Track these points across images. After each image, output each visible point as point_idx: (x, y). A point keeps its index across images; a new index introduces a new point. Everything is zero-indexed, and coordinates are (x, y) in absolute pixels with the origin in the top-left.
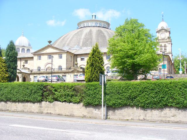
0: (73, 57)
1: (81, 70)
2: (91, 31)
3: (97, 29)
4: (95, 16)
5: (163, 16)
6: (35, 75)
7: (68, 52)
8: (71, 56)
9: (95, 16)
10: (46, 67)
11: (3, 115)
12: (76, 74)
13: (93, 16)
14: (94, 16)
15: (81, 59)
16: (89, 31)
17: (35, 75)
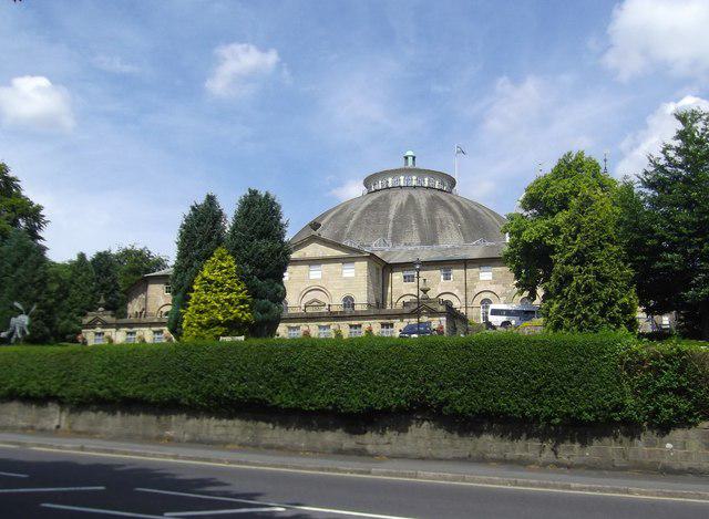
0: (381, 268)
1: (442, 308)
2: (411, 198)
3: (429, 193)
4: (414, 158)
5: (605, 160)
6: (292, 325)
7: (372, 255)
8: (378, 269)
9: (414, 158)
10: (305, 300)
11: (292, 450)
12: (99, 330)
13: (406, 158)
14: (410, 159)
15: (405, 277)
16: (405, 198)
17: (353, 323)
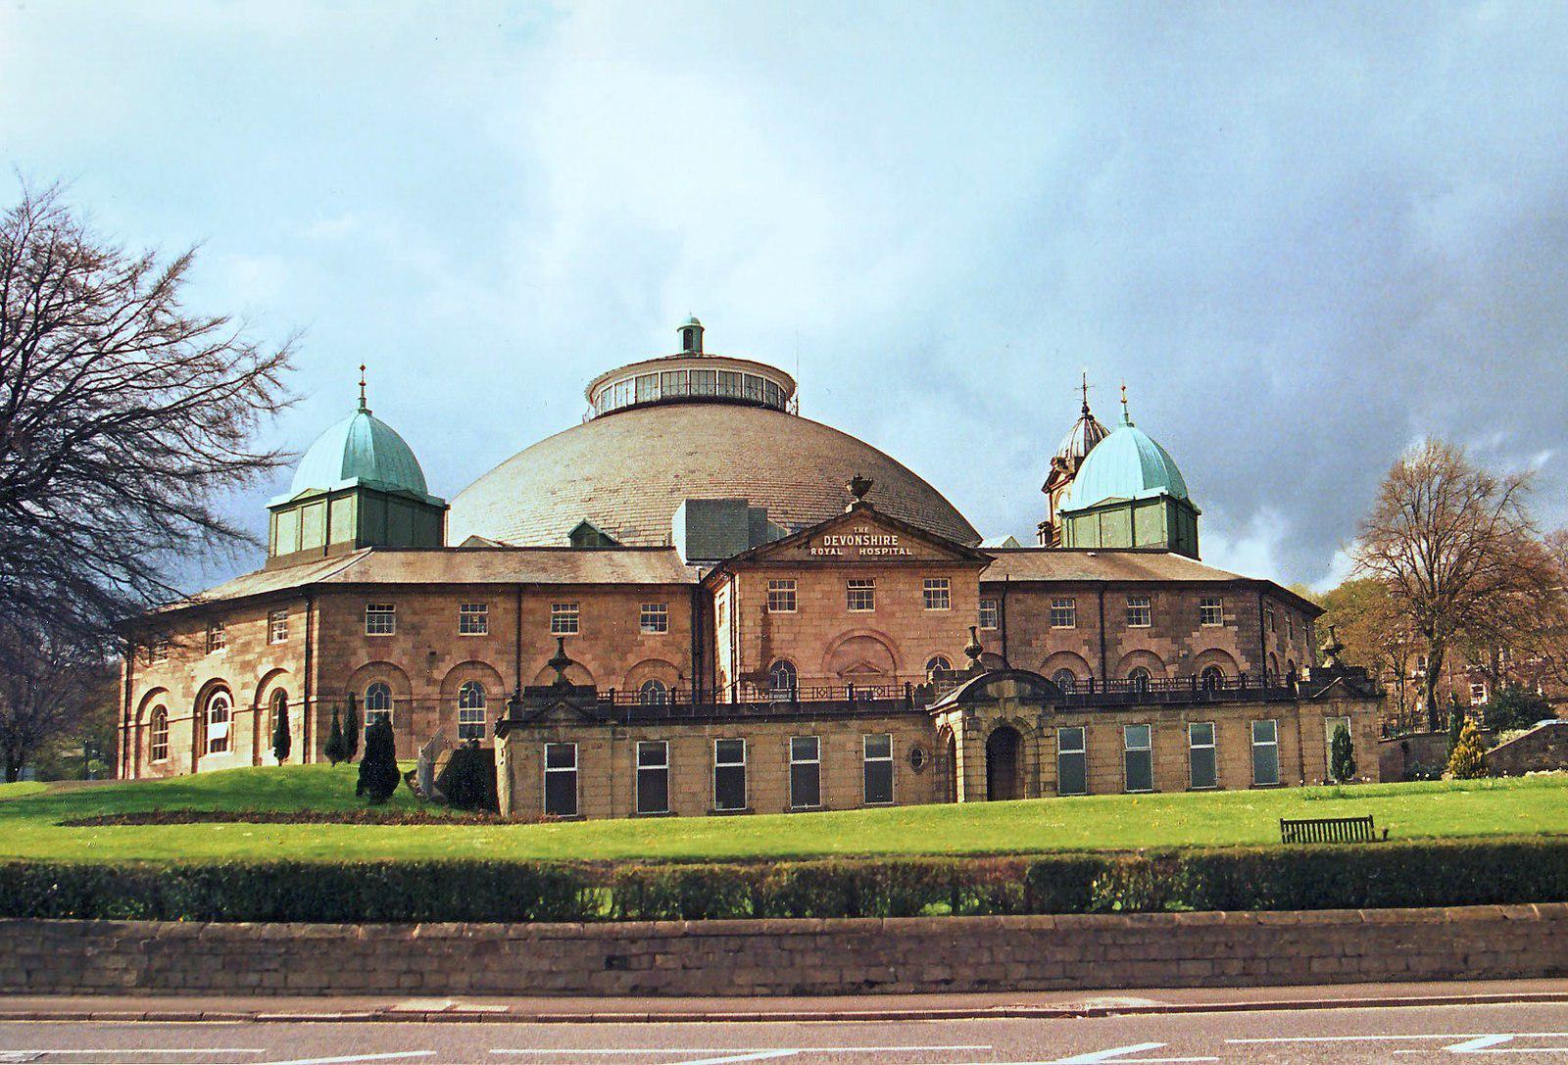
5: (363, 384)
